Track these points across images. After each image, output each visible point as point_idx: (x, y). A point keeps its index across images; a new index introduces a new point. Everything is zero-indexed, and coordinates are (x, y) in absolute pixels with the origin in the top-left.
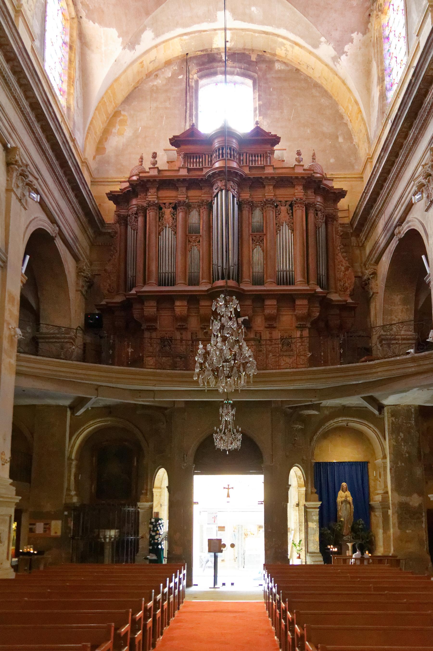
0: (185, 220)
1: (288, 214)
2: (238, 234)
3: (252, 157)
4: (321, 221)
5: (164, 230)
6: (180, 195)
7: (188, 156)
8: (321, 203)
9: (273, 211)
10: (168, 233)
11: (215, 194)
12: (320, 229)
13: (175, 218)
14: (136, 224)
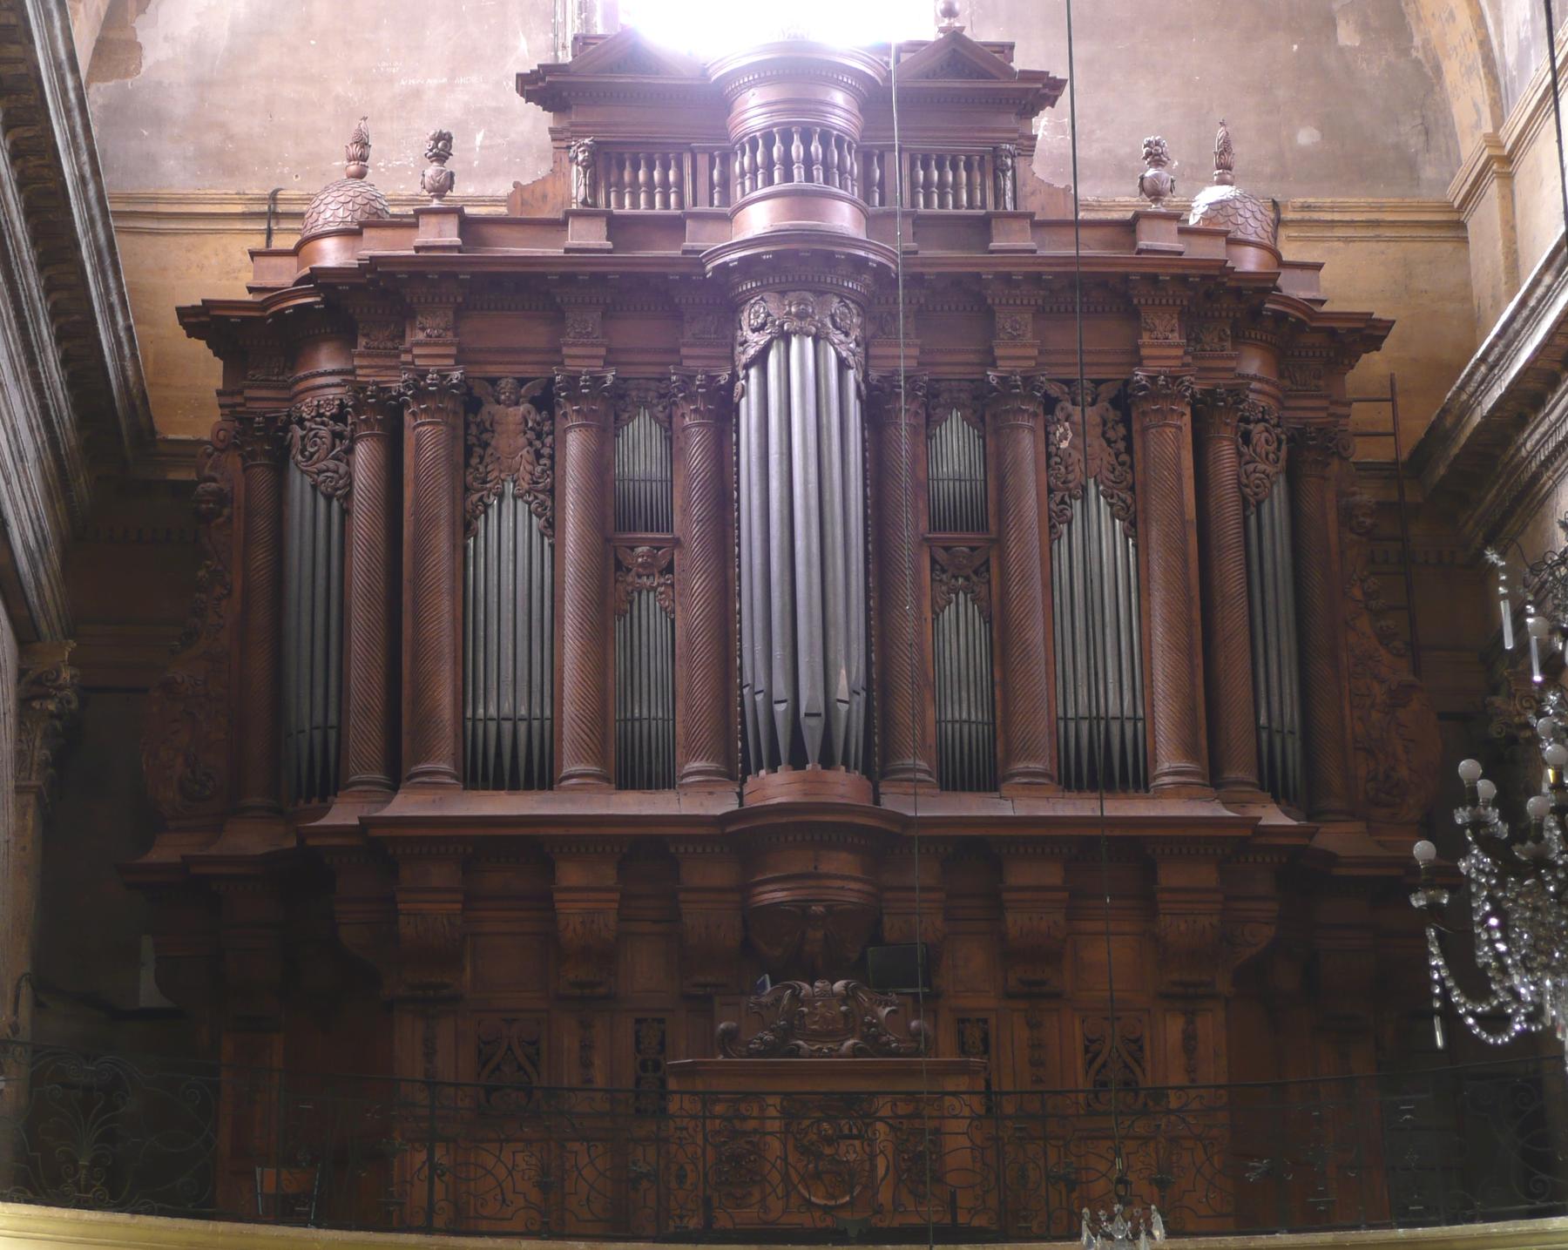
0: (601, 467)
1: (1109, 442)
2: (866, 542)
3: (926, 167)
4: (1270, 470)
5: (493, 513)
6: (574, 345)
7: (607, 162)
8: (1267, 382)
9: (1032, 430)
10: (509, 526)
11: (751, 352)
12: (1265, 508)
13: (546, 451)
14: (343, 468)
